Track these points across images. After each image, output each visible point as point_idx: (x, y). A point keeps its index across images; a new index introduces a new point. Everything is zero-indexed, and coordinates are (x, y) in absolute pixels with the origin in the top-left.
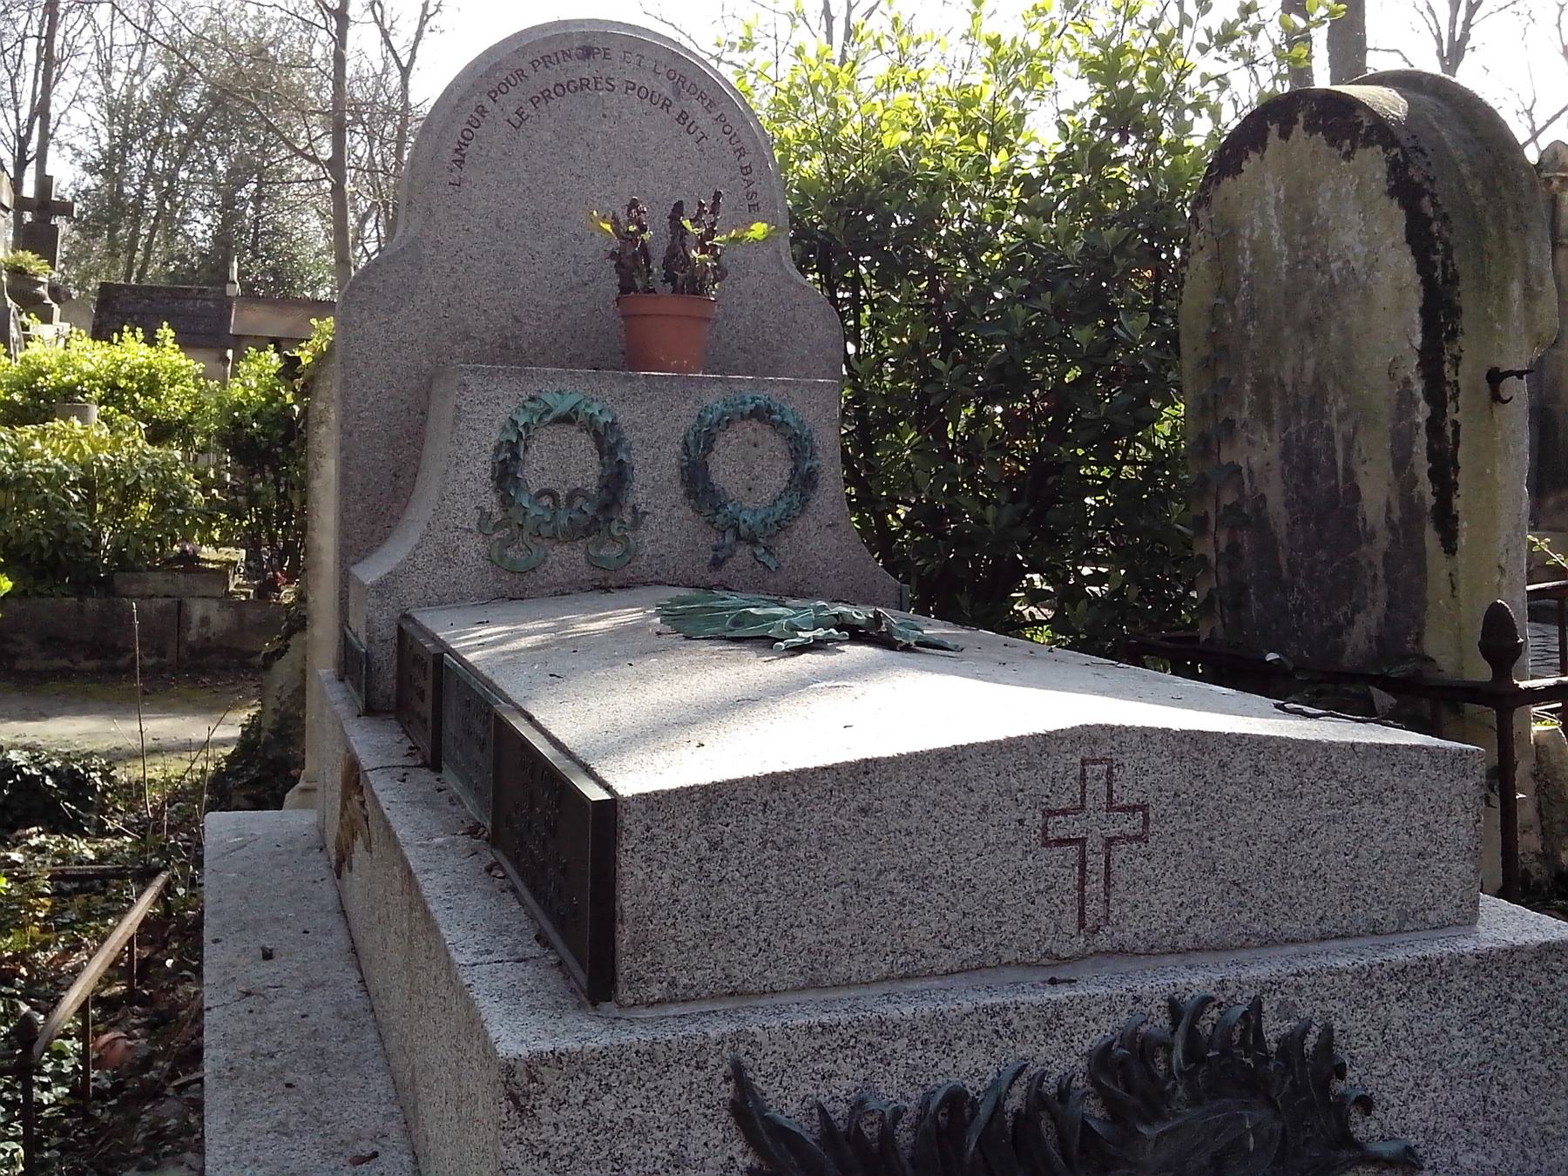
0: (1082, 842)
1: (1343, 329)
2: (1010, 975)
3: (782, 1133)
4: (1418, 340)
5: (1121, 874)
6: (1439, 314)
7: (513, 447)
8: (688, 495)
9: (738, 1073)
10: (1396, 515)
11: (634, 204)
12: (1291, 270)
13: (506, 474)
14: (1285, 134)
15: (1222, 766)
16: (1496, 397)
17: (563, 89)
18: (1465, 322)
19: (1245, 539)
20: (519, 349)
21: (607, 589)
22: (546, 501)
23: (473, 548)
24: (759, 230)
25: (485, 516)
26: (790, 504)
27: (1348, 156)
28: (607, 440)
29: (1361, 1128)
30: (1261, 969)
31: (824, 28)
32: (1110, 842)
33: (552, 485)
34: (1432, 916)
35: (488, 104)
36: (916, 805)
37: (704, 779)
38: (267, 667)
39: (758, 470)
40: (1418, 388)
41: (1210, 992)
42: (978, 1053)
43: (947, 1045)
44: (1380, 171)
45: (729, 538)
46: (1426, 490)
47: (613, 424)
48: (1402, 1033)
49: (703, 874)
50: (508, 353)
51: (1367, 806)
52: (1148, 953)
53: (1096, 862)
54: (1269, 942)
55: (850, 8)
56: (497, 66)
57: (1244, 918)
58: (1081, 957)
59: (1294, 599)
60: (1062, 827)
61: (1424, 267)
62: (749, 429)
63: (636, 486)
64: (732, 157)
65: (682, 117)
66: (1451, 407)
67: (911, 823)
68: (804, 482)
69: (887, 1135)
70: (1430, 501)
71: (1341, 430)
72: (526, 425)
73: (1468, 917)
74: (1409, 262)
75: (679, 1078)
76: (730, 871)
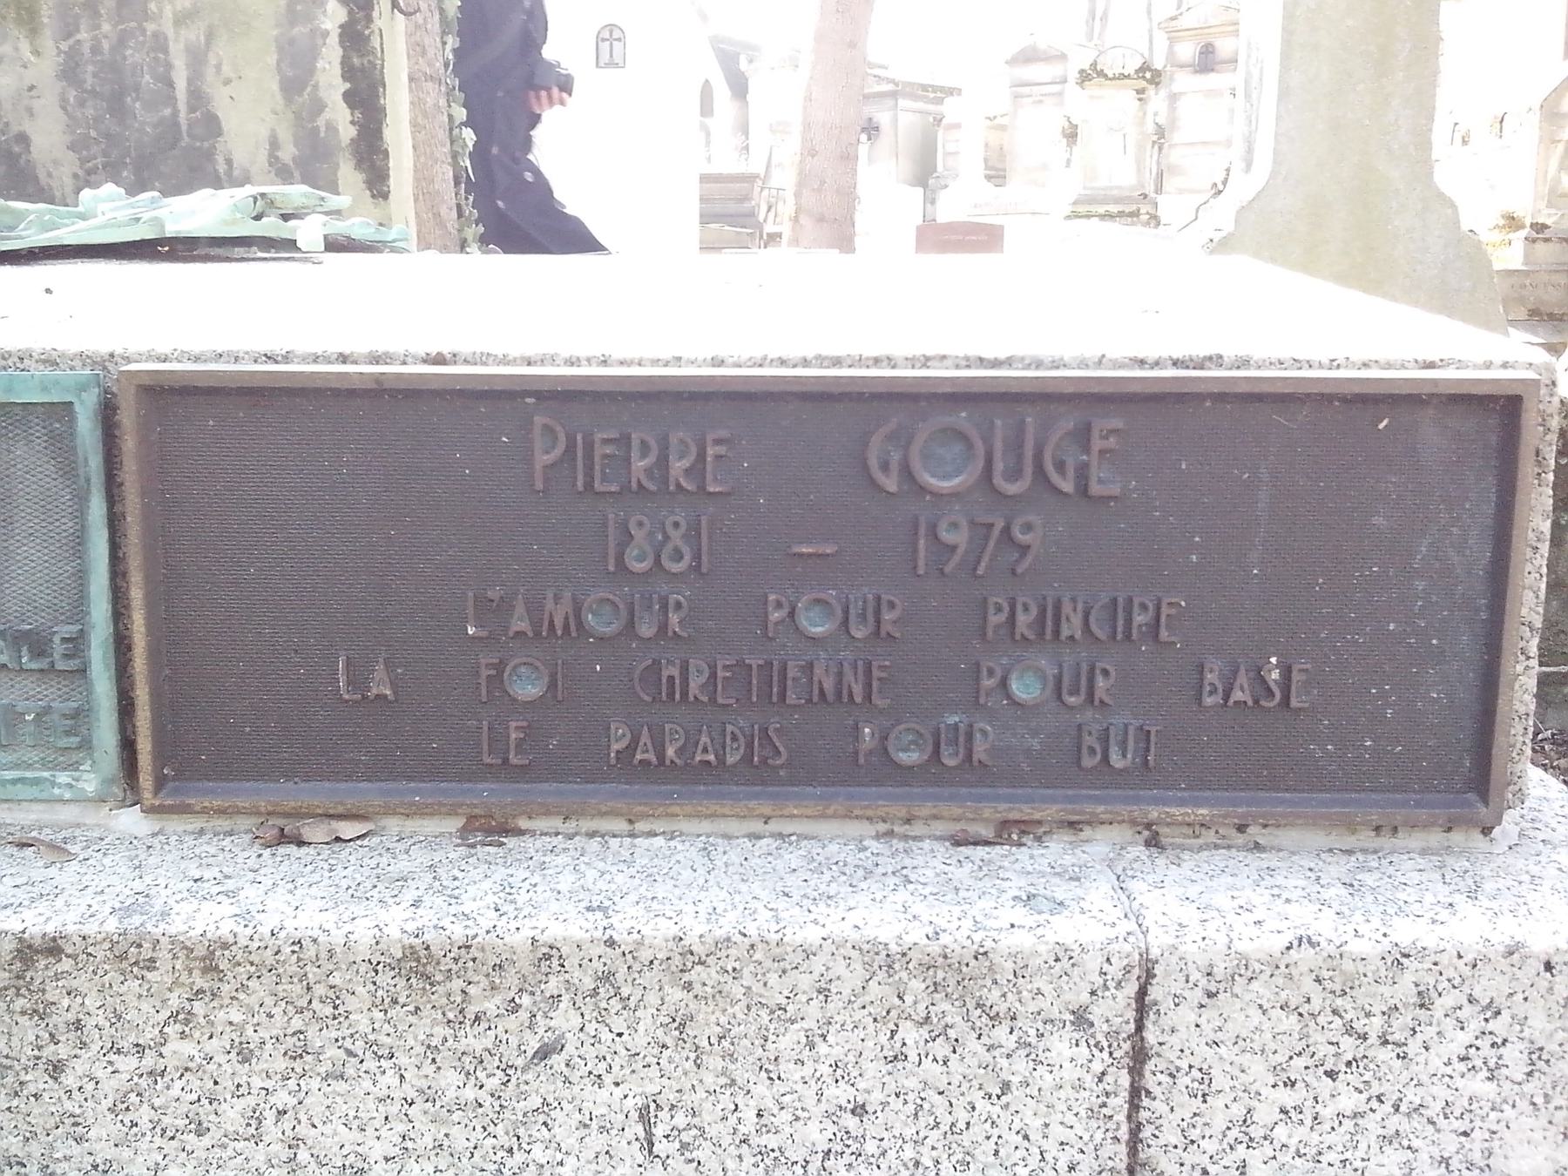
46: (342, 121)
70: (347, 132)
74: (104, 506)
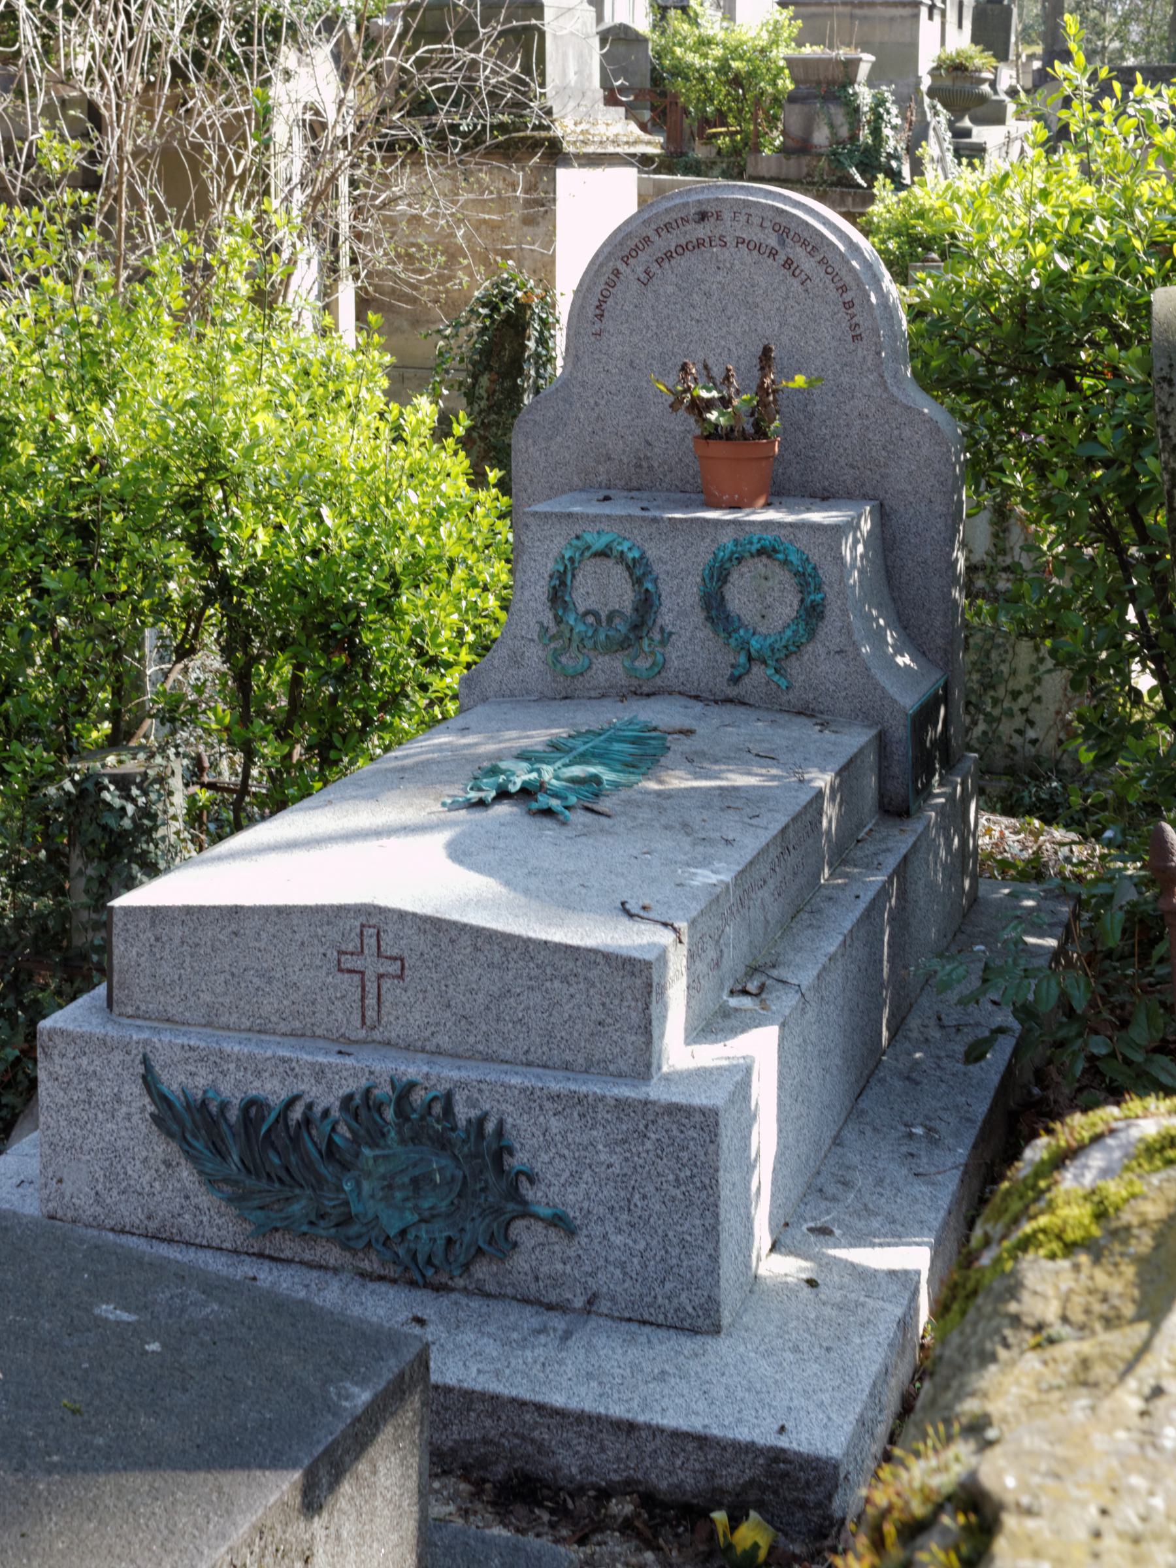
0: (362, 973)
2: (321, 1043)
5: (387, 998)
9: (145, 1061)
13: (558, 595)
15: (452, 941)
17: (683, 249)
20: (651, 467)
22: (591, 619)
26: (795, 632)
28: (638, 571)
29: (529, 1192)
30: (448, 1073)
32: (380, 977)
33: (595, 607)
34: (612, 1068)
35: (622, 267)
36: (264, 935)
37: (153, 903)
39: (769, 600)
41: (419, 1079)
42: (276, 1082)
43: (258, 1074)
47: (642, 557)
48: (558, 1138)
51: (557, 984)
52: (407, 1048)
53: (371, 988)
54: (488, 1059)
56: (629, 235)
57: (472, 1040)
58: (364, 1042)
60: (348, 962)
62: (761, 565)
63: (664, 609)
64: (833, 294)
65: (788, 263)
67: (262, 945)
72: (571, 559)
75: (117, 1057)
76: (166, 954)
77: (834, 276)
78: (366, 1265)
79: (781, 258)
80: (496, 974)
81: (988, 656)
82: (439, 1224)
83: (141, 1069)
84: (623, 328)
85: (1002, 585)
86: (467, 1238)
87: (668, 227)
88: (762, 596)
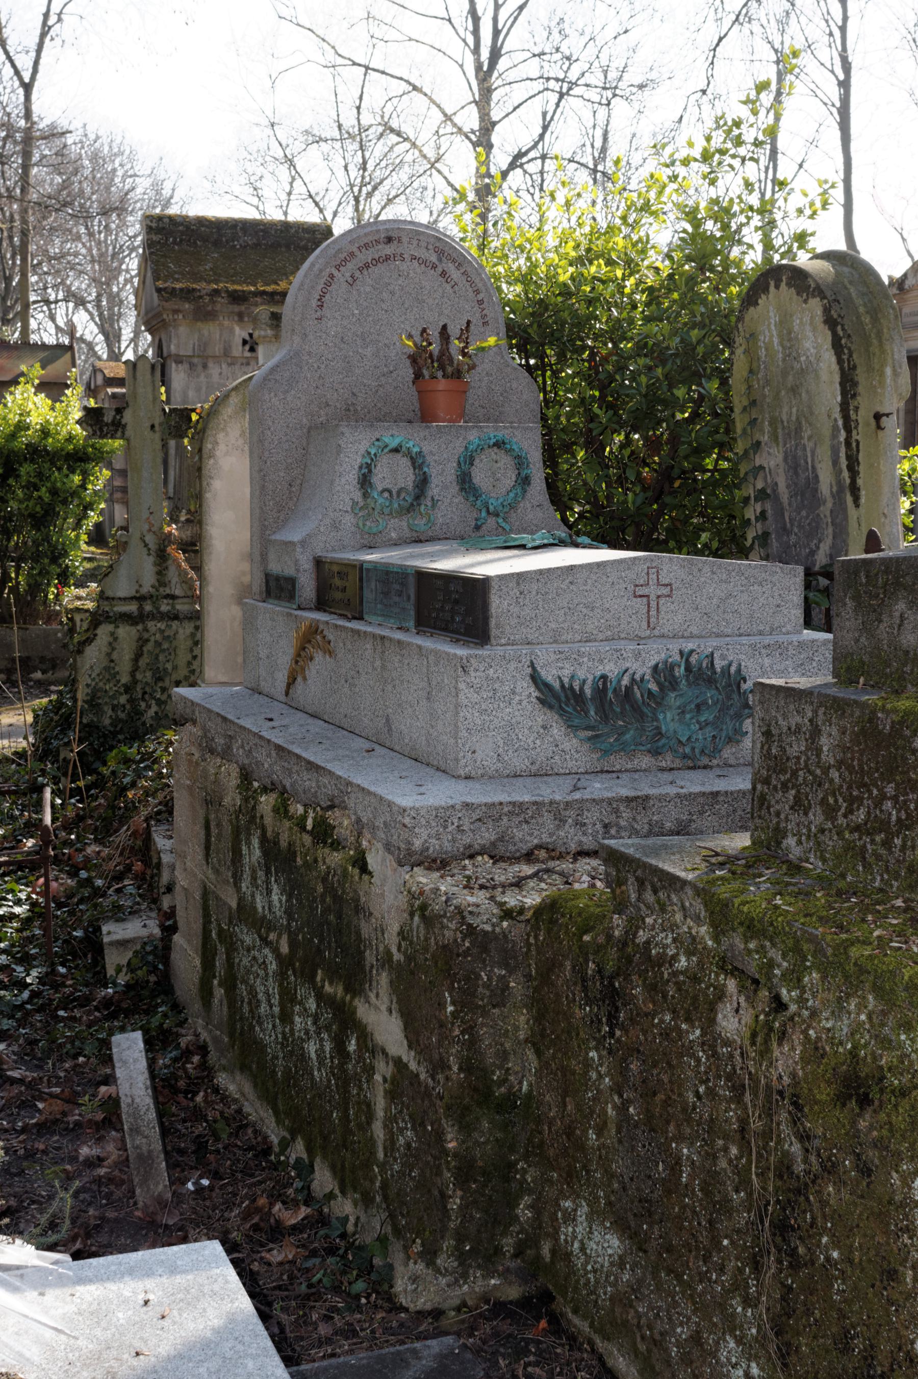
1: (807, 392)
3: (547, 685)
4: (839, 398)
5: (663, 609)
6: (848, 385)
7: (368, 466)
8: (462, 489)
10: (835, 489)
11: (424, 330)
12: (784, 360)
13: (365, 481)
14: (777, 287)
16: (879, 427)
17: (376, 261)
18: (860, 389)
19: (768, 506)
20: (356, 411)
21: (421, 541)
22: (386, 495)
23: (348, 521)
24: (492, 340)
25: (355, 503)
27: (805, 301)
28: (417, 462)
30: (708, 646)
31: (471, 28)
35: (336, 273)
38: (80, 652)
40: (840, 423)
43: (601, 661)
44: (819, 312)
45: (484, 514)
46: (846, 474)
49: (518, 603)
50: (352, 414)
53: (653, 604)
54: (718, 636)
55: (497, 7)
59: (793, 539)
61: (840, 361)
62: (494, 453)
64: (471, 294)
65: (443, 274)
66: (854, 432)
68: (524, 481)
69: (582, 689)
70: (848, 481)
71: (810, 446)
73: (801, 633)
74: (834, 359)
77: (472, 283)
78: (664, 764)
79: (439, 270)
80: (724, 586)
81: (157, 658)
82: (708, 729)
83: (529, 670)
84: (337, 315)
85: (164, 608)
86: (724, 734)
87: (366, 246)
88: (494, 474)
